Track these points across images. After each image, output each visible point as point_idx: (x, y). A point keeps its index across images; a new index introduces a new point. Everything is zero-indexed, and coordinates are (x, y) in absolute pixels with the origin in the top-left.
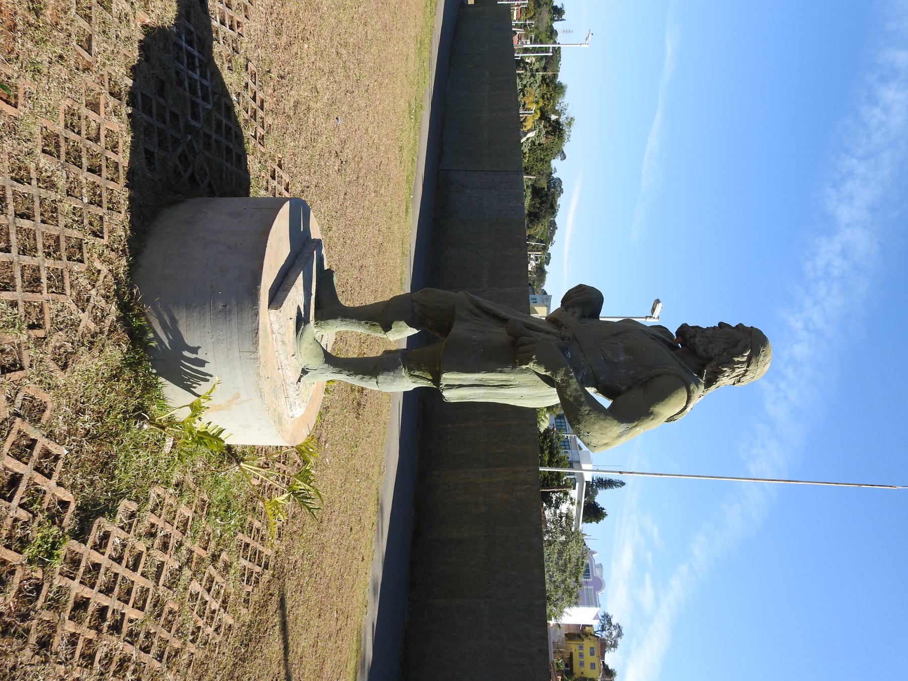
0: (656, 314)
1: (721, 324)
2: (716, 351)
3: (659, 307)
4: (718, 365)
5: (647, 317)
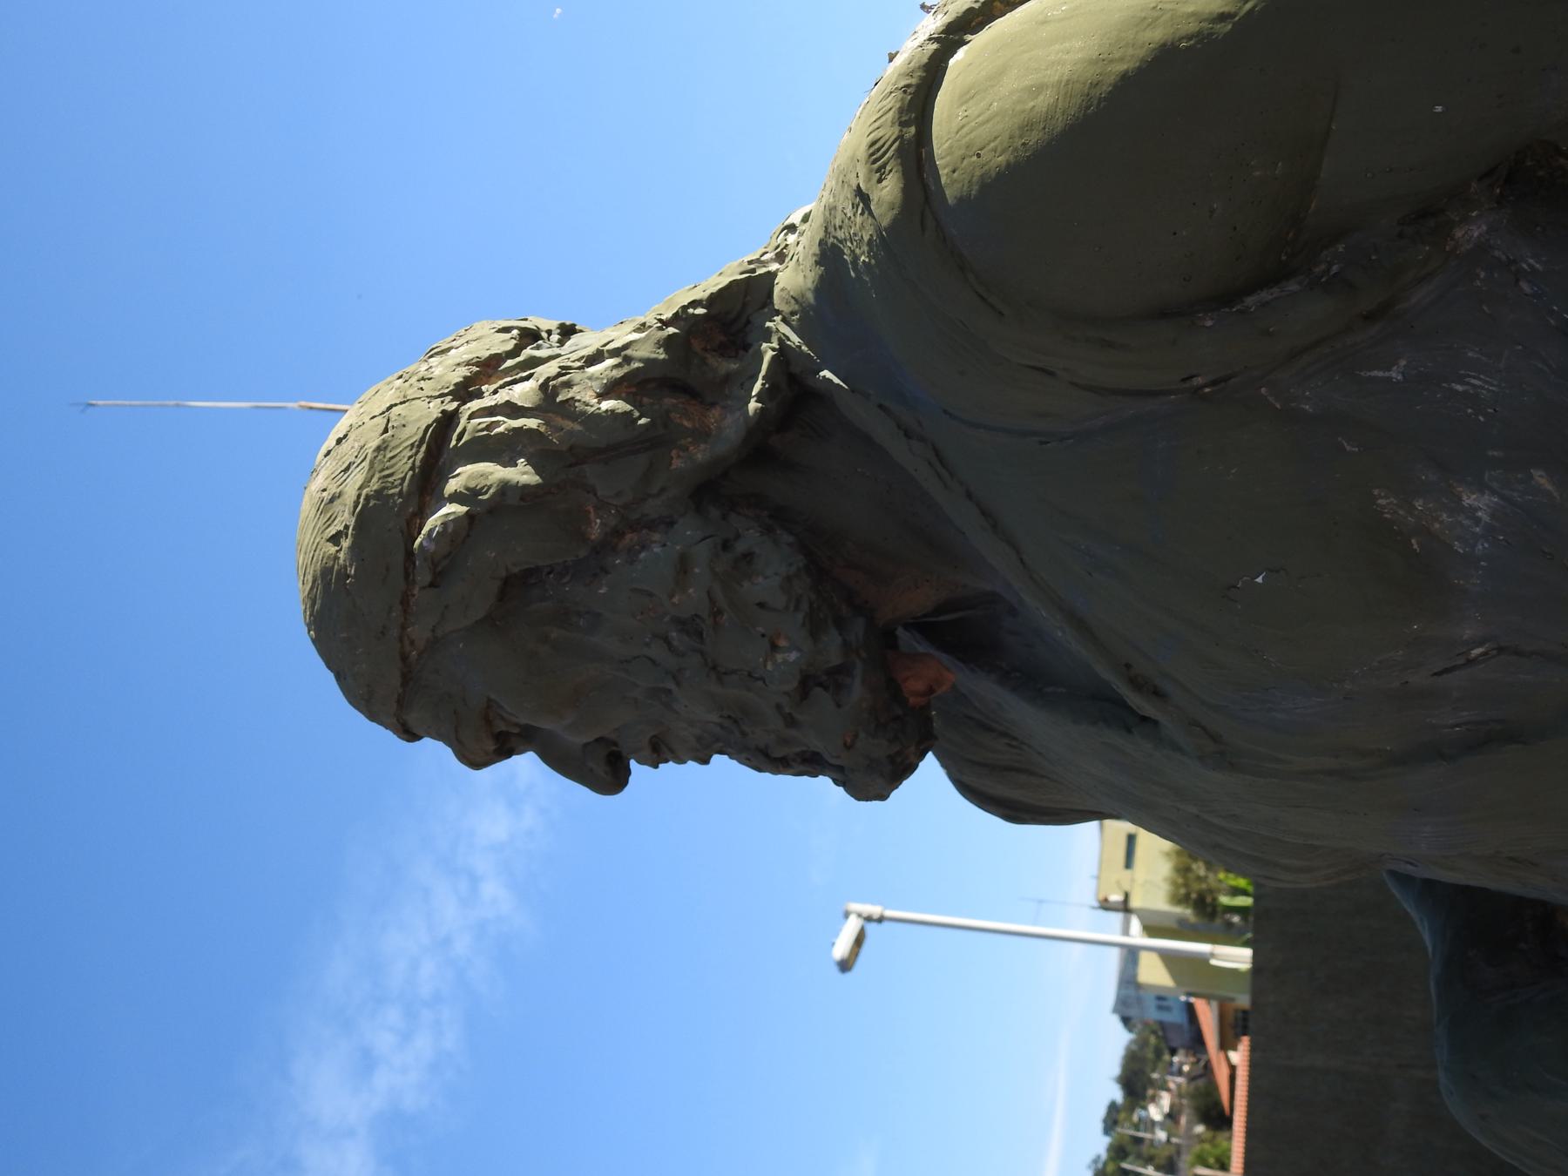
0: (851, 927)
1: (610, 778)
2: (658, 551)
3: (841, 948)
4: (655, 442)
5: (881, 920)
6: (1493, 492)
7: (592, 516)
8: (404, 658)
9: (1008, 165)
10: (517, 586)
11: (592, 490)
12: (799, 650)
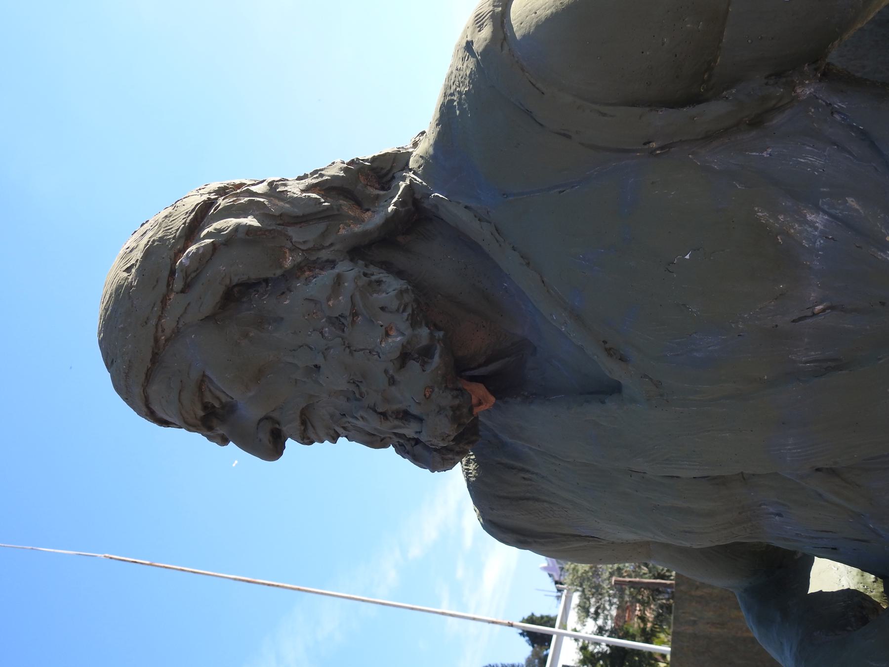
6: (825, 213)
7: (287, 255)
8: (156, 340)
9: (552, 13)
10: (236, 294)
11: (290, 239)
12: (403, 334)
